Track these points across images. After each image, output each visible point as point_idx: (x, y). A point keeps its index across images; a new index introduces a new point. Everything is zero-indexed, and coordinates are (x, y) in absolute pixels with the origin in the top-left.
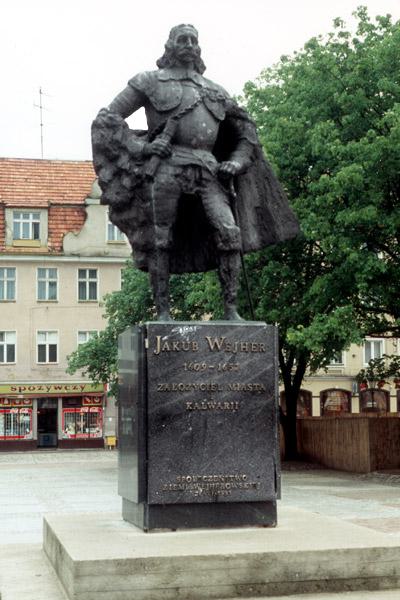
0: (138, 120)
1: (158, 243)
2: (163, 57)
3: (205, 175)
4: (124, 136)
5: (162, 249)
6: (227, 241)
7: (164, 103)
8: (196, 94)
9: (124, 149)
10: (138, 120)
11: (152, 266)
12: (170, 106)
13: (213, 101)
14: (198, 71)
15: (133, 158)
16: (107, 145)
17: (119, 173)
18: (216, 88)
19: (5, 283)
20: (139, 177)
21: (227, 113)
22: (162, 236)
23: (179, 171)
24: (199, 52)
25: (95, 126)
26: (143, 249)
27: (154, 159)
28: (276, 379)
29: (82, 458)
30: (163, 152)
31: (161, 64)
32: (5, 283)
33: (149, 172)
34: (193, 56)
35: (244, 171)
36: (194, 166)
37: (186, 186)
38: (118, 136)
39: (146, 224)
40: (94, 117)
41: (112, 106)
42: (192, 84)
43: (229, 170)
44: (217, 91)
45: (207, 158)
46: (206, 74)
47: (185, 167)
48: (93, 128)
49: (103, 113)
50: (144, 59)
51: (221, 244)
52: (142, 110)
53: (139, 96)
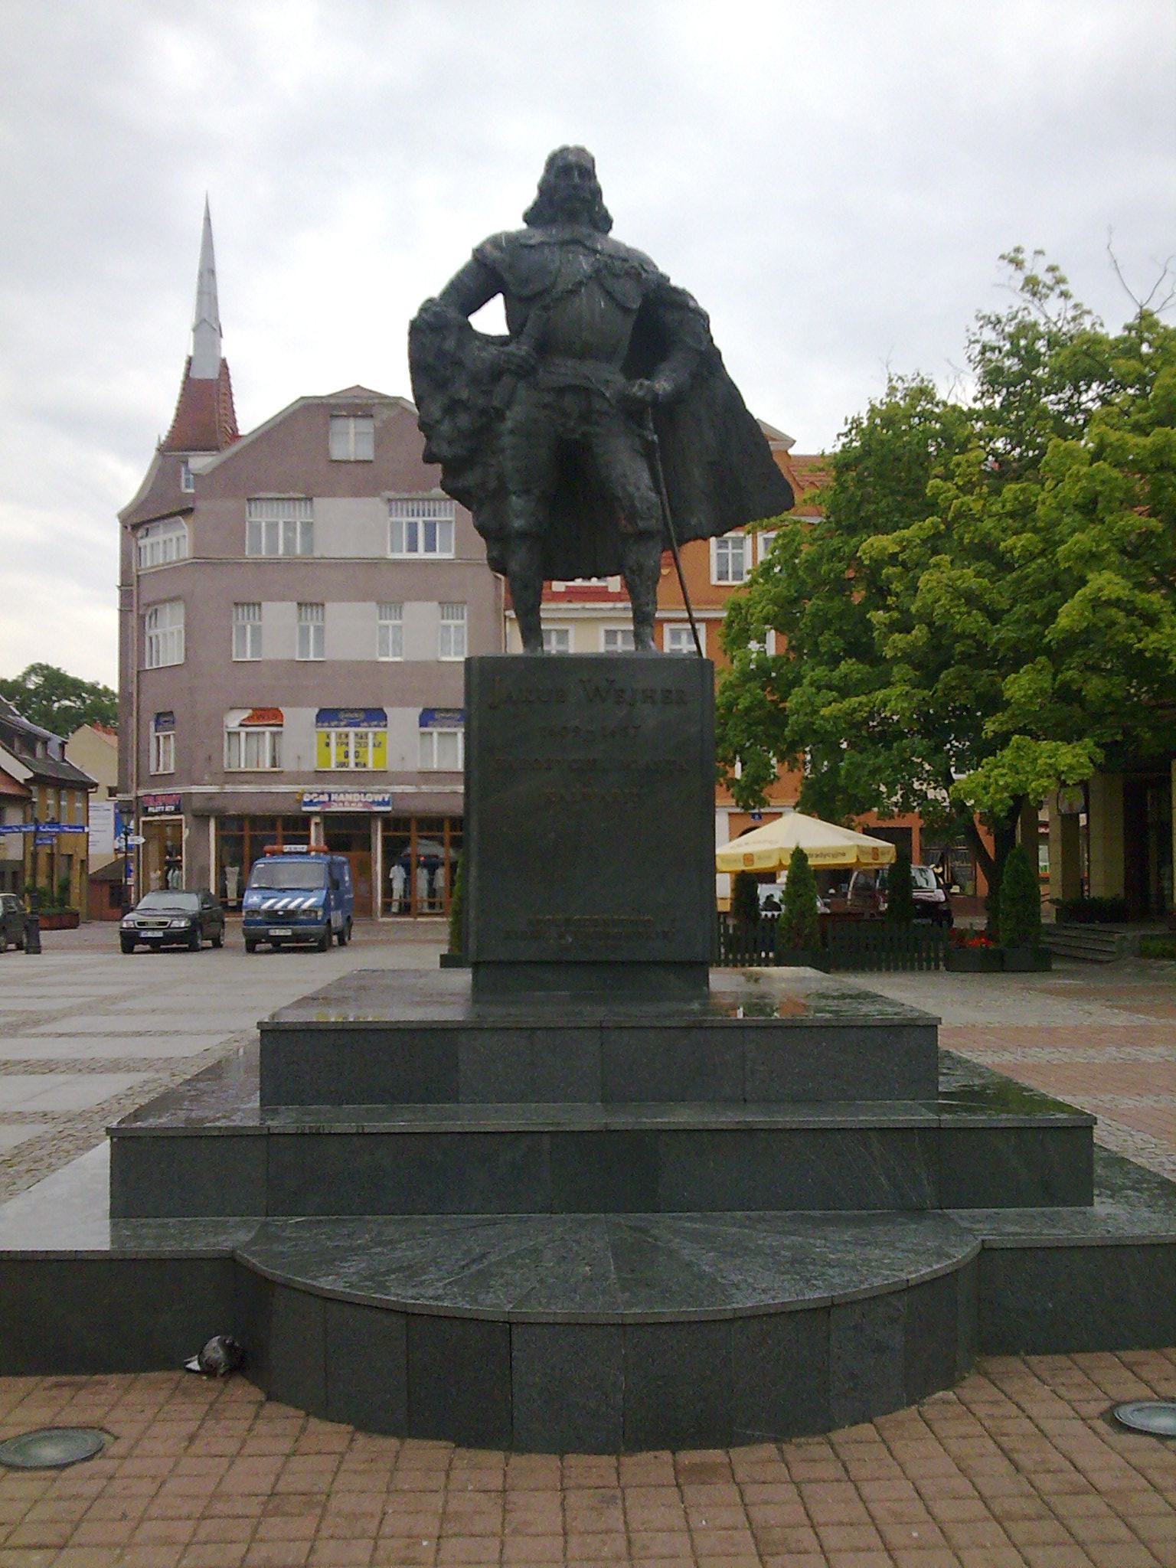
0: (491, 319)
1: (518, 524)
2: (536, 204)
3: (598, 404)
4: (461, 344)
5: (523, 535)
6: (633, 516)
7: (526, 282)
8: (585, 264)
9: (459, 363)
10: (491, 319)
11: (514, 566)
12: (537, 287)
13: (616, 276)
14: (596, 227)
15: (475, 381)
16: (430, 360)
17: (453, 407)
18: (623, 254)
19: (312, 629)
20: (483, 412)
21: (645, 296)
22: (519, 512)
23: (548, 398)
24: (597, 193)
25: (417, 330)
26: (493, 533)
27: (506, 379)
28: (538, 654)
29: (210, 796)
30: (520, 366)
31: (530, 217)
32: (312, 629)
33: (496, 403)
34: (584, 201)
35: (678, 398)
36: (575, 389)
37: (563, 425)
38: (450, 345)
39: (500, 493)
40: (413, 313)
41: (445, 294)
42: (581, 249)
43: (640, 394)
44: (625, 260)
45: (610, 379)
46: (612, 235)
47: (561, 391)
48: (411, 334)
49: (428, 307)
50: (505, 207)
51: (624, 522)
52: (499, 299)
53: (485, 275)
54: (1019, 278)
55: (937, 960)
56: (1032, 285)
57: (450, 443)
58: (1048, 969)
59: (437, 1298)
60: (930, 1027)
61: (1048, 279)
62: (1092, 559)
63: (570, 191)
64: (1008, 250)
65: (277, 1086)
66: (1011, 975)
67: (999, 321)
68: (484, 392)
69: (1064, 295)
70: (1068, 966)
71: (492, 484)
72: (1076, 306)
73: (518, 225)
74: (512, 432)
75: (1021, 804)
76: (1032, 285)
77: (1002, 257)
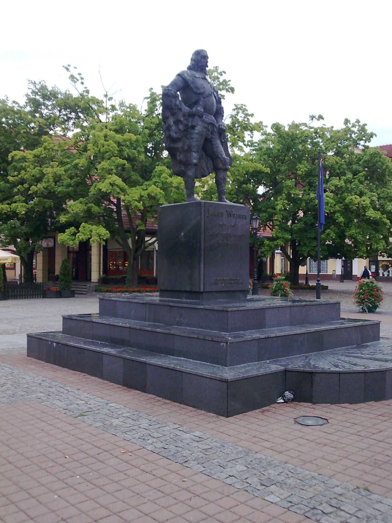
23: (206, 126)
50: (183, 64)
54: (69, 74)
55: (38, 295)
56: (72, 77)
57: (176, 133)
58: (74, 297)
59: (192, 369)
60: (328, 287)
61: (78, 77)
62: (110, 172)
63: (200, 61)
64: (66, 65)
65: (66, 330)
66: (65, 299)
67: (35, 83)
68: (186, 120)
69: (82, 83)
70: (79, 296)
71: (186, 148)
72: (85, 88)
73: (186, 69)
74: (197, 134)
75: (85, 246)
76: (72, 77)
77: (63, 67)
